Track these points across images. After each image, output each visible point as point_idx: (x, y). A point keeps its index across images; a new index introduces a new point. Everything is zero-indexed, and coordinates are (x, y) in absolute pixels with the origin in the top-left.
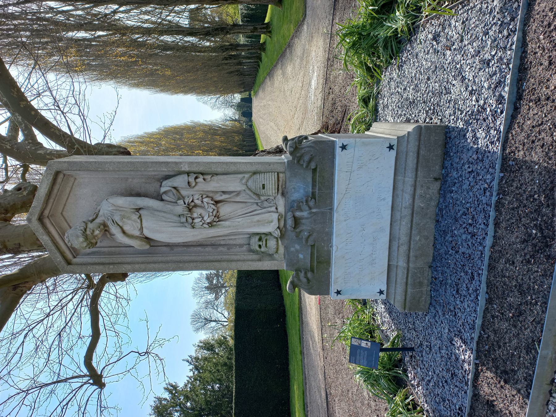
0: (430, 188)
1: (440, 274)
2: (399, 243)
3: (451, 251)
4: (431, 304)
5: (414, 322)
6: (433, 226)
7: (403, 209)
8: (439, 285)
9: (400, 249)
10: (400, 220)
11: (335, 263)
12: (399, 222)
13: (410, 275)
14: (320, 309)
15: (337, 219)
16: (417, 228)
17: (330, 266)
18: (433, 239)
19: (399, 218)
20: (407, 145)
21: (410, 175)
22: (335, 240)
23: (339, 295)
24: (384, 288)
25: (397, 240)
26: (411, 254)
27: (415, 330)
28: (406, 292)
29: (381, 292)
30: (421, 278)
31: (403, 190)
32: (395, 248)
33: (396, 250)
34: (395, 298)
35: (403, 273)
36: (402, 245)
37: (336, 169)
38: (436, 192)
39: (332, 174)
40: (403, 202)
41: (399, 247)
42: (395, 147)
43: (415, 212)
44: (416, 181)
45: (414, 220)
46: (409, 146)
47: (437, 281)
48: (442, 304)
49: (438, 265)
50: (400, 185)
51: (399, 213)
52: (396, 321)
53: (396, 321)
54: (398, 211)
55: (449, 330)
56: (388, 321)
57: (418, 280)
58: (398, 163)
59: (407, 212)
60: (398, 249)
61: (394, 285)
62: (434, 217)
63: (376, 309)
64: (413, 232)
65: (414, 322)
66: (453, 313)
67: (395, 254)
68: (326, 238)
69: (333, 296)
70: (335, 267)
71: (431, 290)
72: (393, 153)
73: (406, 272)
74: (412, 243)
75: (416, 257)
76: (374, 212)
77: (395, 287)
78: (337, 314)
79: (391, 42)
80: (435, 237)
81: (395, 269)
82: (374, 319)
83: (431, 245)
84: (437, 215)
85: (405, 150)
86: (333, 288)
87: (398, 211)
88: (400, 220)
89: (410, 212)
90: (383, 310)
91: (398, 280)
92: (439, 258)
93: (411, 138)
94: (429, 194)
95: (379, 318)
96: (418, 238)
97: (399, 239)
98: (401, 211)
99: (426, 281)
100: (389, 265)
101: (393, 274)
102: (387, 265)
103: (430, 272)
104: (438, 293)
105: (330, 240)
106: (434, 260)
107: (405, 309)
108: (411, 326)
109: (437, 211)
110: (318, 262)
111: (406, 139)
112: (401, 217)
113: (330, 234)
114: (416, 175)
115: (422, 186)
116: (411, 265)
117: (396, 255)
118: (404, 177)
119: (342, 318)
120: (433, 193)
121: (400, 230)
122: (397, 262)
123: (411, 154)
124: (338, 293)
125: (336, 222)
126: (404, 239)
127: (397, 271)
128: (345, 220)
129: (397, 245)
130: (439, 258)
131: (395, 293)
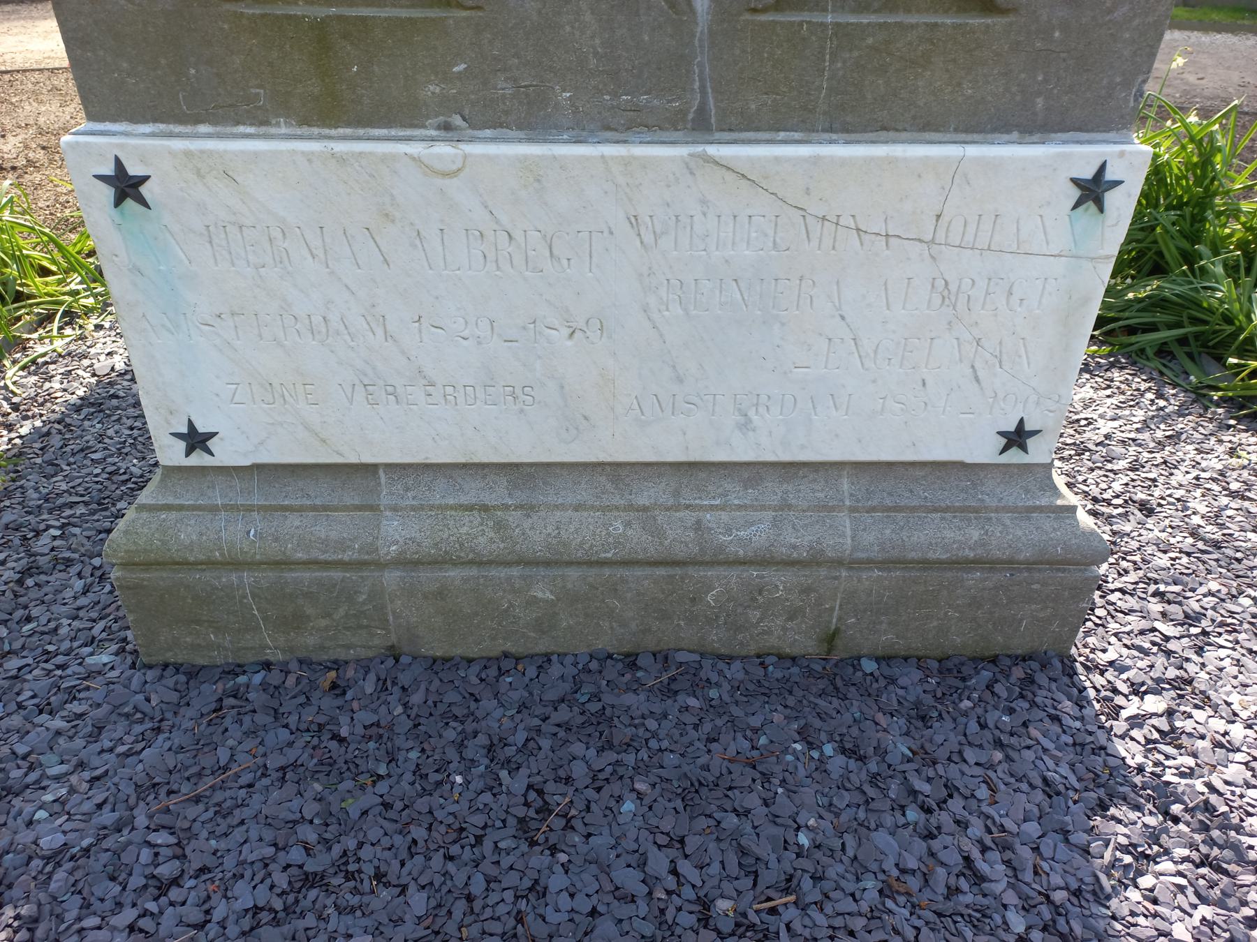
0: (791, 619)
1: (367, 717)
2: (506, 507)
3: (517, 784)
4: (194, 673)
5: (68, 563)
6: (604, 643)
7: (690, 517)
8: (309, 715)
9: (476, 517)
10: (630, 507)
11: (342, 160)
12: (617, 500)
13: (336, 575)
14: (52, 70)
15: (645, 163)
16: (592, 587)
17: (305, 121)
18: (541, 648)
19: (643, 500)
20: (1014, 510)
21: (869, 538)
22: (499, 154)
23: (108, 192)
24: (225, 453)
25: (521, 496)
26: (454, 574)
27: (26, 572)
28: (235, 564)
29: (196, 440)
30: (323, 623)
31: (785, 506)
32: (473, 492)
33: (464, 500)
34: (180, 508)
35: (342, 545)
36: (500, 526)
37: (972, 151)
38: (772, 641)
39: (927, 124)
40: (724, 516)
41: (485, 508)
42: (1014, 456)
43: (678, 571)
44: (838, 563)
45: (639, 572)
46: (1007, 518)
47: (328, 702)
48: (207, 761)
49: (416, 698)
50: (806, 492)
51: (666, 499)
52: (56, 441)
53: (56, 441)
54: (676, 493)
55: (55, 858)
56: (50, 398)
57: (309, 611)
58: (919, 473)
59: (677, 534)
60: (470, 508)
61: (257, 500)
62: (651, 643)
63: (98, 327)
64: (573, 573)
65: (68, 563)
66: (166, 870)
67: (440, 494)
68: (503, 86)
69: (94, 146)
70: (309, 157)
71: (267, 665)
72: (985, 450)
73: (347, 556)
74: (515, 572)
75: (441, 594)
76: (680, 380)
77: (249, 509)
78: (42, 141)
79: (1170, 327)
80: (548, 657)
81: (352, 499)
82: (49, 318)
83: (509, 646)
84: (663, 658)
85: (991, 502)
86: (143, 147)
87: (676, 493)
88: (630, 507)
89: (680, 552)
90: (102, 365)
91: (294, 520)
92: (451, 697)
93: (1047, 523)
94: (761, 620)
95: (59, 344)
96: (542, 593)
97: (529, 509)
98: (676, 508)
99: (311, 641)
100: (369, 470)
101: (321, 493)
102: (367, 458)
103: (364, 653)
104: (261, 718)
105: (492, 117)
106: (435, 664)
107: (125, 565)
108: (42, 544)
109: (682, 657)
110: (320, 26)
111: (1044, 502)
112: (645, 509)
113: (531, 117)
114: (869, 563)
115: (807, 590)
116: (391, 578)
117: (437, 499)
118: (853, 510)
119: (30, 163)
120: (768, 632)
121: (577, 508)
122: (395, 509)
123: (975, 534)
124: (126, 187)
125: (627, 162)
126: (537, 532)
127: (346, 508)
128: (634, 221)
129: (489, 499)
130: (451, 697)
131: (214, 509)
